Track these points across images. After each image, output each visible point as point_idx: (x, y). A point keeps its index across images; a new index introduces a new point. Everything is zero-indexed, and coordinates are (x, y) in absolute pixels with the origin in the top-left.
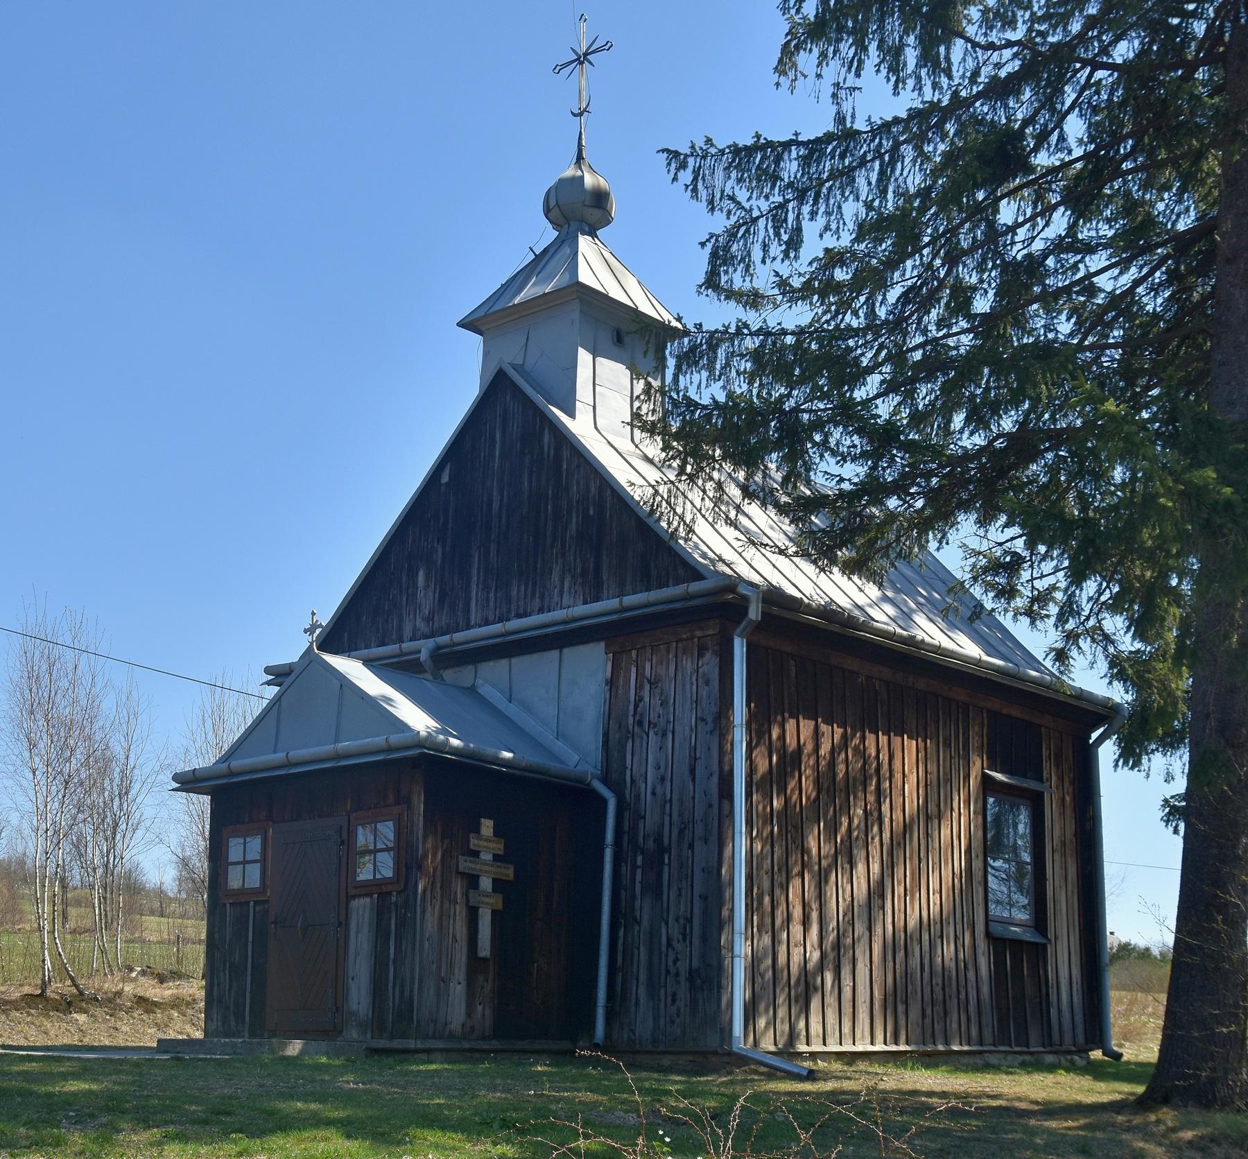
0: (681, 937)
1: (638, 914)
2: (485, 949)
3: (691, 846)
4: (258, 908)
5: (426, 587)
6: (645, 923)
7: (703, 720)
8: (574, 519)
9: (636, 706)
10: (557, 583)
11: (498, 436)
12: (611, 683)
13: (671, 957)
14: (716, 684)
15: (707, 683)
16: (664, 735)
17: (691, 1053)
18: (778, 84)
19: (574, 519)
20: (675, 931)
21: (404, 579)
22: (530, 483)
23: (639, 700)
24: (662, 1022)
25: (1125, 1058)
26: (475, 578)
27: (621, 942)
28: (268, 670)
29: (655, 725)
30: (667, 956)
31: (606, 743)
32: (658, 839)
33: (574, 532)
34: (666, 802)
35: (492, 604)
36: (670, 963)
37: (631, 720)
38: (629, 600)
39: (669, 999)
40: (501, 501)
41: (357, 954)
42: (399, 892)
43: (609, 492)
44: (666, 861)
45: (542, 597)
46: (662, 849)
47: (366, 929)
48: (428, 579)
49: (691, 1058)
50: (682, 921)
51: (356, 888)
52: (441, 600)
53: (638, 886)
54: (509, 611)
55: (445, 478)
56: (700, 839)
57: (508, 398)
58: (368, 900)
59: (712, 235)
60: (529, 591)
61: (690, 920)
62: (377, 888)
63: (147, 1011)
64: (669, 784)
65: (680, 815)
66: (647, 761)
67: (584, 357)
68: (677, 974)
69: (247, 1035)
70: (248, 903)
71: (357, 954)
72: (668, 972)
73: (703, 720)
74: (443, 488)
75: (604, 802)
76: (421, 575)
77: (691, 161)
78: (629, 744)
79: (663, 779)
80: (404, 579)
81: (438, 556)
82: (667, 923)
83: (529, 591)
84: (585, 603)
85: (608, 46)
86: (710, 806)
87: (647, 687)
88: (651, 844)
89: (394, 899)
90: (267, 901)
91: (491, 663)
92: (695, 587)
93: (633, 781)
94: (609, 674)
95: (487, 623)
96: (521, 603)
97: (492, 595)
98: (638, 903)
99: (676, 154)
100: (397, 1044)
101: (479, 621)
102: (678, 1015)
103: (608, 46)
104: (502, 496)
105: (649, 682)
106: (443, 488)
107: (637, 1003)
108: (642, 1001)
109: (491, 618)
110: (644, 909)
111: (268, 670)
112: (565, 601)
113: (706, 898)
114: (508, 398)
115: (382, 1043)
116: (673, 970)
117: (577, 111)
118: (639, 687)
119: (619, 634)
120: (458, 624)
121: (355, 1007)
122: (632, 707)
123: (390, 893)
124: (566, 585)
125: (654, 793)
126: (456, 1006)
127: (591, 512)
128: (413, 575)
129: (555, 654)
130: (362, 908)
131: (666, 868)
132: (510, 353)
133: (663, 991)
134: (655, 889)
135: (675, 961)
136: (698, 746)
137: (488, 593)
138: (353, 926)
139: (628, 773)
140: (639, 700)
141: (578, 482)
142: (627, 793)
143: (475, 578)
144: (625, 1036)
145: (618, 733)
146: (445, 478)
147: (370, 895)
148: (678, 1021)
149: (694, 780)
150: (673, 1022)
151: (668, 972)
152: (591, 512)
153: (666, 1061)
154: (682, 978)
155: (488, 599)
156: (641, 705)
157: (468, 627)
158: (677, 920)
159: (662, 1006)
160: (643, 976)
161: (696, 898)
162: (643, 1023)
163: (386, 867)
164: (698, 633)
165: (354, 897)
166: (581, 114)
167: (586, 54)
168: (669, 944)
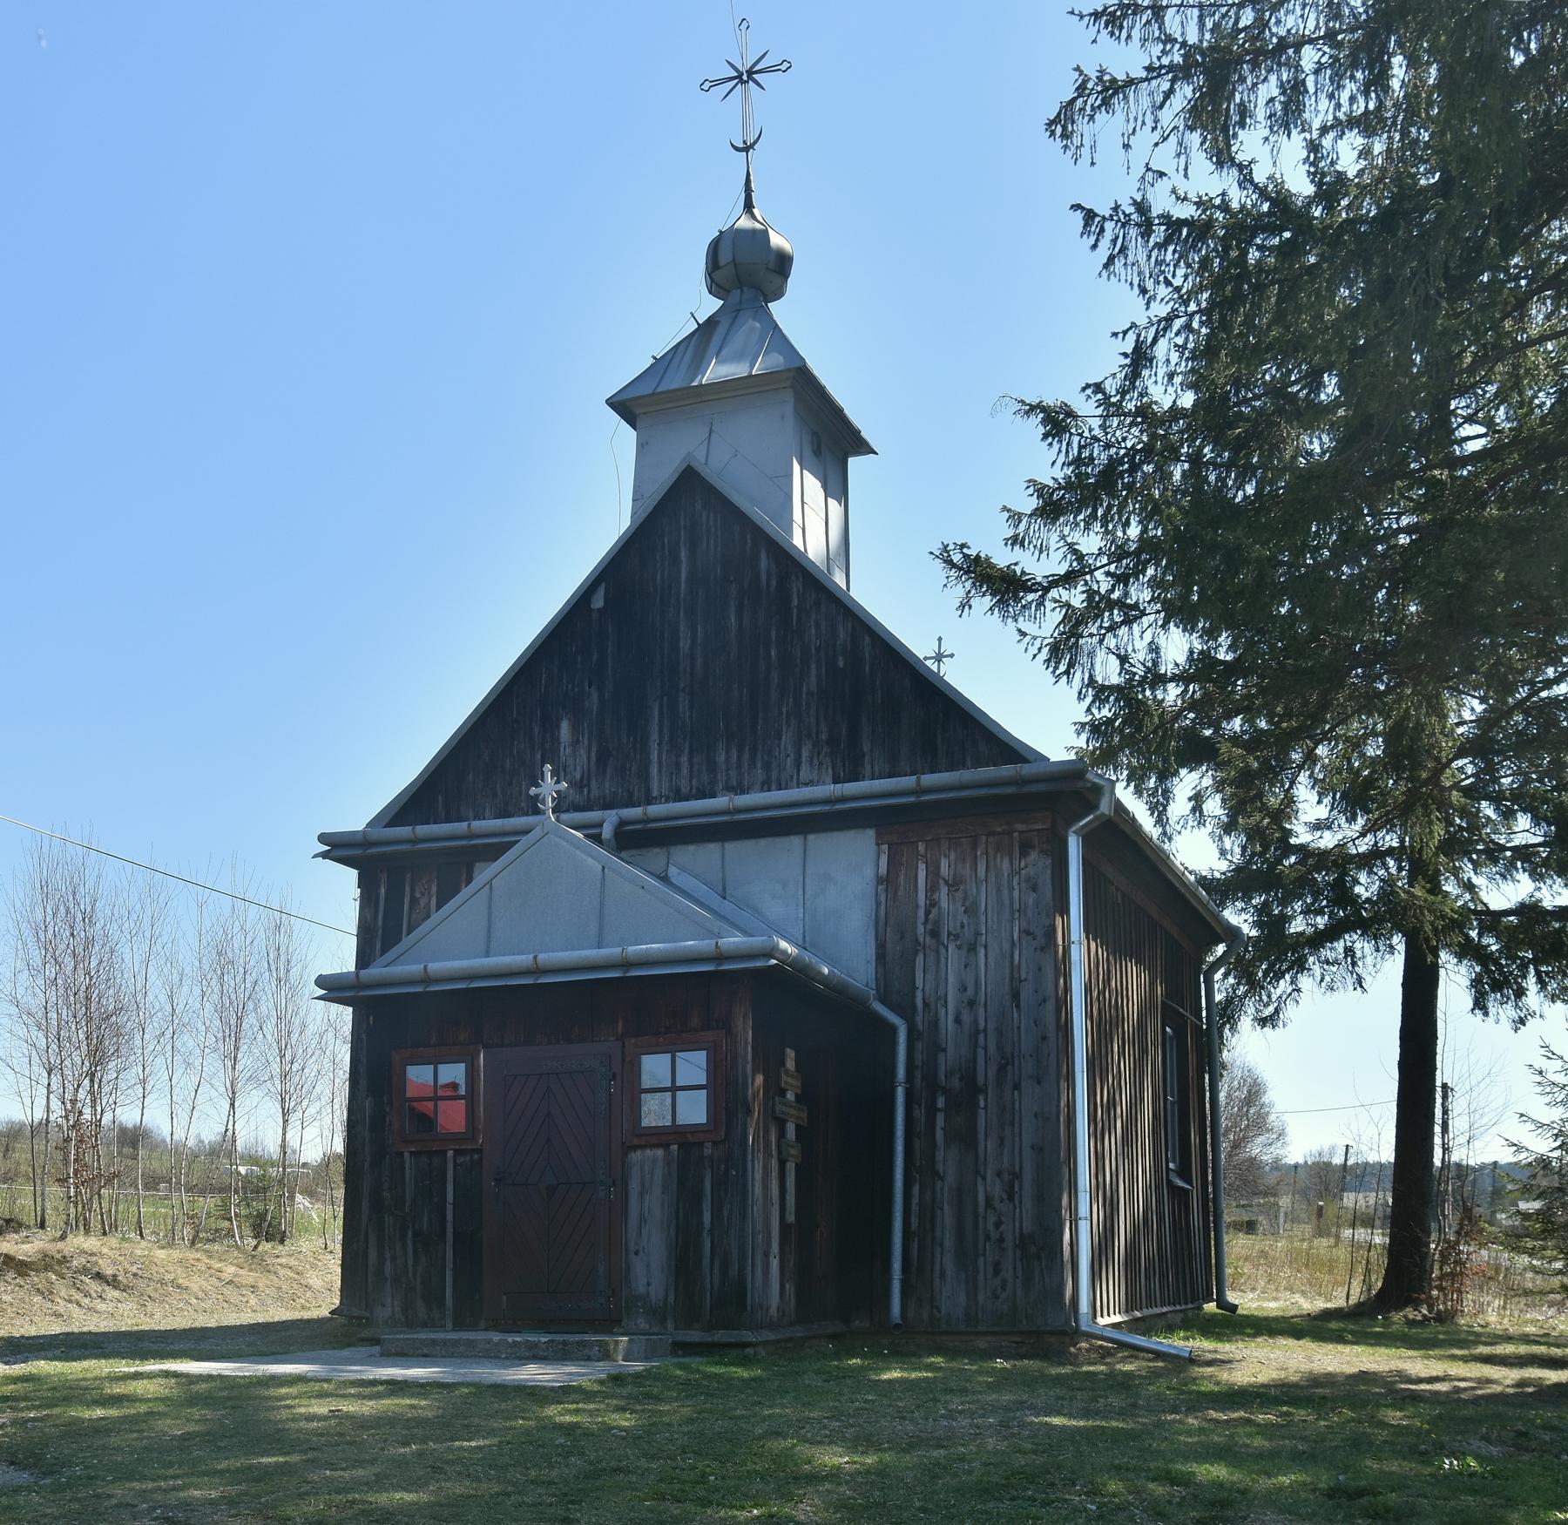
0: (1005, 1196)
1: (940, 1167)
2: (791, 1218)
3: (1017, 1086)
4: (460, 1160)
5: (575, 743)
6: (951, 1177)
7: (1028, 933)
8: (813, 672)
9: (927, 913)
10: (790, 750)
11: (683, 554)
12: (887, 882)
13: (992, 1219)
14: (1048, 890)
15: (1034, 888)
16: (972, 948)
17: (1020, 1333)
18: (1267, 139)
19: (813, 672)
20: (997, 1190)
21: (536, 730)
22: (740, 618)
23: (932, 904)
24: (981, 1297)
25: (1240, 1311)
26: (655, 736)
27: (915, 1201)
28: (323, 838)
29: (957, 937)
30: (985, 1218)
31: (881, 955)
32: (969, 1076)
33: (814, 688)
34: (977, 1032)
35: (685, 772)
36: (991, 1227)
37: (921, 929)
38: (929, 779)
39: (990, 1270)
40: (694, 638)
41: (642, 1220)
42: (715, 1143)
43: (867, 640)
44: (982, 1104)
45: (767, 767)
46: (972, 1088)
47: (657, 1190)
48: (575, 729)
49: (1018, 1339)
50: (1006, 1176)
51: (638, 1136)
52: (603, 759)
53: (939, 1134)
54: (713, 782)
55: (598, 602)
56: (1030, 1077)
57: (699, 507)
58: (660, 1153)
59: (1133, 325)
60: (746, 756)
61: (1016, 1176)
62: (677, 1137)
63: (22, 1274)
64: (981, 1011)
65: (999, 1047)
66: (947, 979)
67: (796, 467)
68: (1001, 1240)
69: (449, 1325)
70: (445, 1152)
71: (642, 1220)
72: (988, 1238)
73: (1028, 933)
74: (595, 615)
75: (893, 1030)
76: (565, 729)
77: (1109, 226)
78: (920, 960)
79: (972, 1004)
80: (536, 730)
81: (593, 701)
82: (984, 1178)
83: (746, 756)
84: (836, 781)
85: (783, 67)
86: (1044, 1038)
87: (944, 889)
88: (956, 1083)
89: (708, 1151)
90: (479, 1151)
91: (692, 848)
92: (1007, 770)
93: (926, 1005)
94: (883, 870)
95: (679, 797)
96: (733, 773)
97: (684, 759)
98: (940, 1155)
99: (1090, 215)
100: (720, 1336)
101: (665, 791)
102: (1003, 1289)
103: (783, 67)
104: (694, 633)
105: (946, 882)
106: (595, 615)
107: (943, 1275)
108: (948, 1272)
109: (685, 789)
110: (948, 1162)
111: (323, 838)
112: (805, 773)
113: (1041, 1150)
114: (699, 507)
115: (694, 1336)
116: (994, 1235)
117: (741, 145)
118: (932, 888)
119: (894, 824)
120: (631, 794)
121: (642, 1290)
122: (921, 913)
123: (701, 1144)
124: (805, 754)
125: (958, 1021)
126: (771, 1286)
127: (841, 664)
128: (550, 726)
129: (796, 841)
130: (649, 1165)
131: (982, 1112)
132: (685, 444)
133: (981, 1260)
134: (966, 1139)
135: (998, 1224)
136: (1023, 965)
137: (678, 756)
138: (634, 1186)
139: (919, 995)
140: (932, 904)
141: (818, 626)
142: (919, 1018)
143: (655, 736)
144: (925, 1315)
145: (899, 944)
146: (598, 602)
147: (666, 1146)
148: (1003, 1295)
149: (1018, 1006)
150: (996, 1297)
151: (988, 1238)
152: (841, 664)
153: (982, 1343)
154: (1009, 1244)
155: (678, 765)
156: (934, 911)
157: (650, 801)
158: (999, 1175)
159: (981, 1277)
160: (949, 1242)
161: (1027, 1151)
162: (951, 1297)
163: (694, 1110)
164: (1020, 827)
165: (635, 1148)
166: (747, 149)
167: (750, 73)
168: (989, 1204)
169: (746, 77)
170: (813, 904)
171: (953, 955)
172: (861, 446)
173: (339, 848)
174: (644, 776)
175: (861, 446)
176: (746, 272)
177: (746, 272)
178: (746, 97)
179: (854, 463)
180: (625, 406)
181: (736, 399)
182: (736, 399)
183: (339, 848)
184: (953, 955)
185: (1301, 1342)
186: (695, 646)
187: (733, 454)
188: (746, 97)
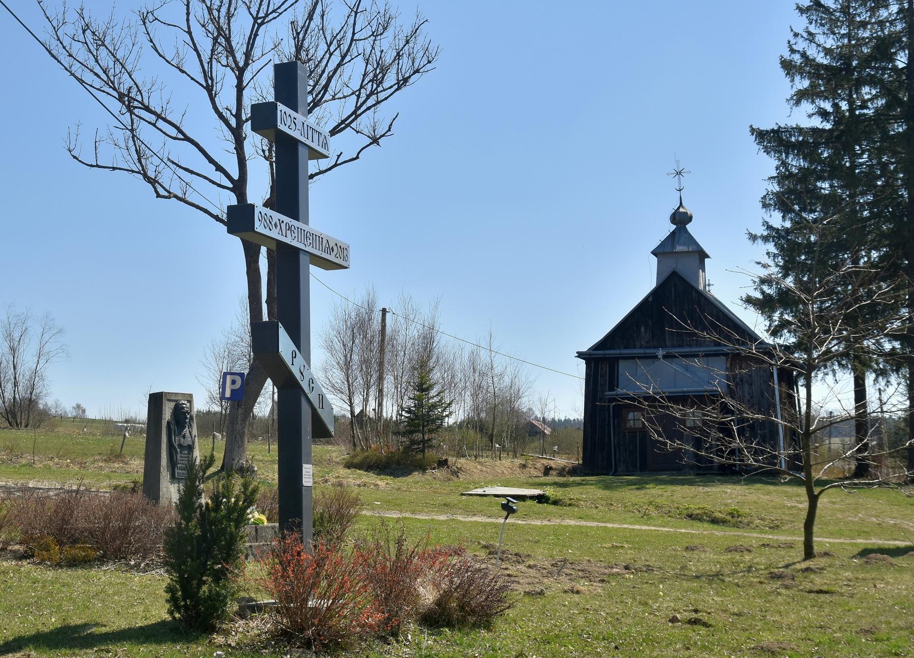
5: (646, 332)
16: (751, 385)
48: (646, 329)
76: (643, 329)
146: (650, 299)
166: (680, 190)
169: (679, 173)
170: (714, 376)
171: (746, 386)
172: (708, 257)
173: (580, 355)
174: (665, 342)
175: (708, 257)
176: (681, 219)
177: (681, 219)
178: (679, 178)
179: (689, 227)
180: (654, 253)
181: (680, 254)
182: (680, 254)
183: (580, 355)
184: (746, 386)
185: (409, 479)
186: (676, 309)
187: (684, 267)
188: (679, 178)
